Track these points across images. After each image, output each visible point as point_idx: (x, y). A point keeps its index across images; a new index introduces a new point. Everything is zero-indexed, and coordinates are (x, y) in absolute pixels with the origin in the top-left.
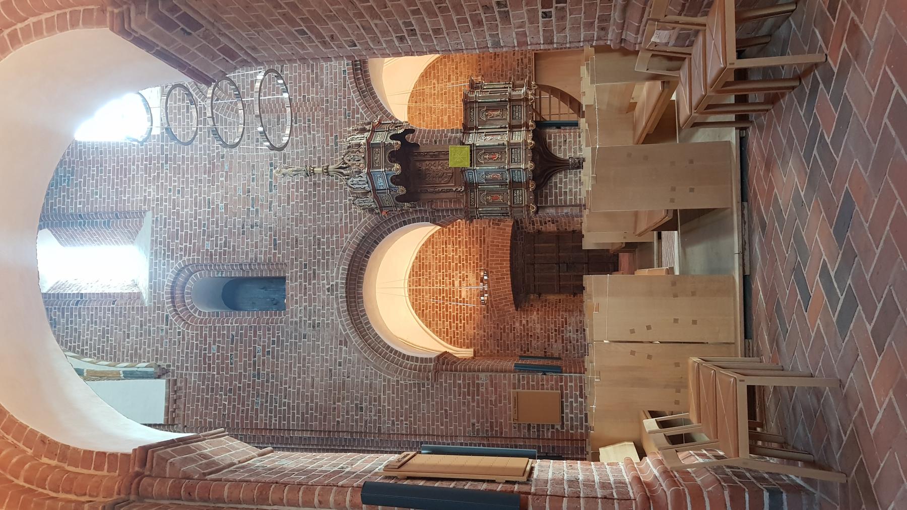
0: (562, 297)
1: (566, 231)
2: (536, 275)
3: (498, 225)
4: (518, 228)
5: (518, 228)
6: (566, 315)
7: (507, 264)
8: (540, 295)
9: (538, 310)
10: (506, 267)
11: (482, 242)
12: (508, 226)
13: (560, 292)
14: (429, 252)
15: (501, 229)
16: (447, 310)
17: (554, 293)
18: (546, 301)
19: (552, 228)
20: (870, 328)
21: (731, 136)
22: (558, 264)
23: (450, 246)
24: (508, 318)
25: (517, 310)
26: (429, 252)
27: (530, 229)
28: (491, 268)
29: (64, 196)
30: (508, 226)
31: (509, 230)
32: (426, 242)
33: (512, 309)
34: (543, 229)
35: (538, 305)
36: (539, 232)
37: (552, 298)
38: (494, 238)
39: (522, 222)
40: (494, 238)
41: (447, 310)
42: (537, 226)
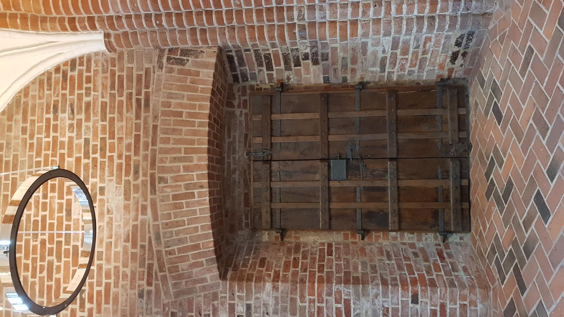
0: (336, 238)
1: (344, 85)
2: (276, 185)
3: (181, 62)
4: (236, 78)
5: (236, 78)
6: (347, 291)
7: (201, 160)
8: (283, 232)
9: (276, 278)
10: (198, 167)
11: (143, 105)
12: (205, 65)
13: (329, 228)
14: (16, 131)
15: (189, 73)
16: (50, 277)
17: (314, 228)
18: (297, 247)
19: (311, 75)
20: (501, 217)
21: (332, 161)
22: (326, 160)
23: (64, 116)
24: (199, 299)
25: (223, 276)
26: (16, 131)
27: (263, 78)
28: (163, 170)
29: (186, 169)
30: (205, 65)
31: (207, 75)
32: (10, 106)
33: (211, 274)
34: (293, 80)
35: (278, 259)
36: (283, 87)
37: (312, 240)
38: (170, 96)
39: (242, 62)
40: (170, 96)
41: (50, 277)
42: (279, 72)
